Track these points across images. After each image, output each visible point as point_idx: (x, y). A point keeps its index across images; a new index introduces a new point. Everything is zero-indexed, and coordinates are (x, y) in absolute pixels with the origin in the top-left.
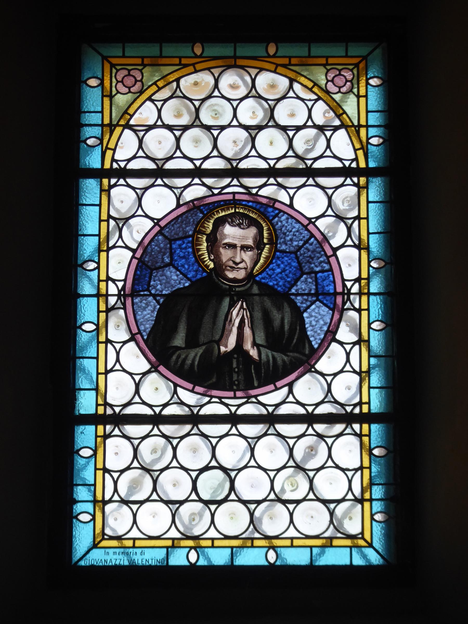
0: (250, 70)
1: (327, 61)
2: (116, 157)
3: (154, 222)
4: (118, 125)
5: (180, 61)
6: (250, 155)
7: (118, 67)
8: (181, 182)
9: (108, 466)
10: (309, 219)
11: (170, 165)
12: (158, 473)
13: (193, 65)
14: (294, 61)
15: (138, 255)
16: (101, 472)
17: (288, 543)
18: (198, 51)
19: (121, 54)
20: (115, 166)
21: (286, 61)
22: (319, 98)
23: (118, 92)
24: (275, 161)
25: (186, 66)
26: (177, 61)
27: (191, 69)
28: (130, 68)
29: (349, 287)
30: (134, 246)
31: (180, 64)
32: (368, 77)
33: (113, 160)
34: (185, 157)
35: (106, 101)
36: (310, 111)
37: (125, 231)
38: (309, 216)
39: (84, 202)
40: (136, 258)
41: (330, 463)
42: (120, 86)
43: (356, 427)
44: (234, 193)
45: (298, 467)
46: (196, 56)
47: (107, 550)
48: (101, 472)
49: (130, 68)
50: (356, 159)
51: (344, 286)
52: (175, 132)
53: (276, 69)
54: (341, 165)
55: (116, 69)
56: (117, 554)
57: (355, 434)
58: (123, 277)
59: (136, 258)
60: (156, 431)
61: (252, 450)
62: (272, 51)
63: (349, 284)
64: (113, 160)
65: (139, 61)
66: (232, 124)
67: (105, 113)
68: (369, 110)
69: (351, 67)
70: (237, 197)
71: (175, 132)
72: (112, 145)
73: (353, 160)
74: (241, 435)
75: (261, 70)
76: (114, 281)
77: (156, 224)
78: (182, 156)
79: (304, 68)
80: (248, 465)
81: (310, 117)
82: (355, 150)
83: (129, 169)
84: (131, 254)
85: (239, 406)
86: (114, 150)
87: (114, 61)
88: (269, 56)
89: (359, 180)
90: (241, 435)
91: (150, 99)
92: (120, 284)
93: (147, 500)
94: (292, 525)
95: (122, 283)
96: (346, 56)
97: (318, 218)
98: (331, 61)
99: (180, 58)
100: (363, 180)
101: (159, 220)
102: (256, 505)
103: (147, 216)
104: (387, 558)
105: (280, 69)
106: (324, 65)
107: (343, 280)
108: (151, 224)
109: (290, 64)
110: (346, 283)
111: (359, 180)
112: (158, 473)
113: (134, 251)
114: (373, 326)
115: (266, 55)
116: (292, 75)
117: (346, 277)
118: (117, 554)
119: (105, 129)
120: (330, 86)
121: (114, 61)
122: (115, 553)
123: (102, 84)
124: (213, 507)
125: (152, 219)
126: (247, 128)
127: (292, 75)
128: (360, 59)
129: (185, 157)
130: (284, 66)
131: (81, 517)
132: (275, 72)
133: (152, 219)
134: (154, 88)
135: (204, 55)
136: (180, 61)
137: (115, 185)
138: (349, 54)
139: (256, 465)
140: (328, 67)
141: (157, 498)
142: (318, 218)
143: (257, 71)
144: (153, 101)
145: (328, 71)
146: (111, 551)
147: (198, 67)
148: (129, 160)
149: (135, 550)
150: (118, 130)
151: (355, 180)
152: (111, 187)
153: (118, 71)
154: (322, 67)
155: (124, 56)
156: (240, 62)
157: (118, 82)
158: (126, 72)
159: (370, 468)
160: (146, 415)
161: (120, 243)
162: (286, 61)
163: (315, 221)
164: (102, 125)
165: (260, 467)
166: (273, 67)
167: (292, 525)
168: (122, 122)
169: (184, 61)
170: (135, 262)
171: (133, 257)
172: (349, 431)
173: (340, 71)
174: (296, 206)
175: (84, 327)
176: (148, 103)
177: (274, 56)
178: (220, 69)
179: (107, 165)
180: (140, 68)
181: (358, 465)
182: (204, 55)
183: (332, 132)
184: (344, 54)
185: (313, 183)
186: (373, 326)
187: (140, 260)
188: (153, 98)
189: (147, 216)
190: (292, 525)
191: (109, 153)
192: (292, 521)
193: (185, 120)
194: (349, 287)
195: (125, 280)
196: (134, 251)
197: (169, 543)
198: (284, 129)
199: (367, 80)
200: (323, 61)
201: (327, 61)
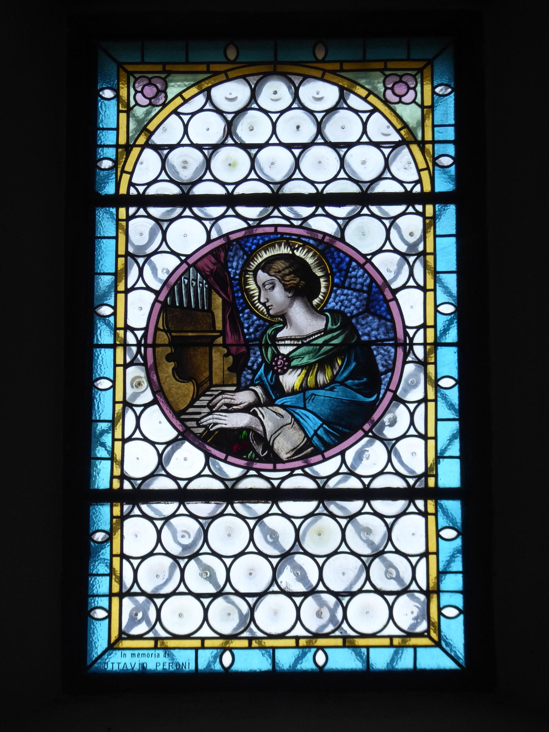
0: (293, 78)
1: (385, 65)
2: (134, 181)
3: (180, 259)
4: (135, 145)
5: (208, 68)
6: (159, 179)
7: (137, 76)
8: (215, 211)
9: (126, 552)
10: (364, 256)
11: (199, 190)
12: (363, 558)
13: (225, 72)
14: (346, 66)
15: (161, 298)
16: (119, 558)
17: (245, 643)
18: (232, 54)
19: (139, 60)
20: (133, 191)
21: (336, 66)
22: (375, 110)
23: (137, 104)
24: (324, 185)
25: (216, 73)
26: (203, 68)
27: (223, 77)
28: (400, 73)
29: (411, 336)
30: (157, 286)
31: (208, 71)
32: (435, 84)
33: (131, 184)
34: (216, 180)
35: (123, 116)
36: (365, 124)
37: (147, 270)
38: (364, 252)
39: (102, 234)
40: (159, 302)
41: (344, 548)
42: (139, 96)
43: (420, 503)
44: (276, 226)
45: (379, 554)
46: (229, 62)
47: (124, 652)
48: (119, 558)
49: (150, 76)
50: (419, 181)
51: (406, 334)
52: (383, 149)
53: (323, 75)
54: (401, 190)
55: (134, 77)
56: (136, 655)
57: (420, 513)
58: (144, 325)
59: (159, 302)
60: (182, 510)
61: (206, 532)
62: (320, 55)
63: (411, 332)
64: (131, 184)
65: (159, 68)
66: (362, 141)
67: (120, 130)
68: (435, 124)
69: (414, 73)
70: (280, 230)
71: (383, 149)
72: (129, 168)
73: (416, 182)
74: (284, 515)
75: (305, 78)
76: (133, 330)
77: (182, 262)
78: (212, 179)
79: (362, 74)
80: (339, 551)
81: (365, 132)
82: (419, 171)
83: (148, 195)
84: (152, 296)
85: (283, 479)
86: (132, 174)
87: (130, 68)
88: (318, 61)
89: (424, 209)
90: (284, 515)
91: (175, 112)
92: (140, 334)
93: (174, 593)
94: (391, 621)
95: (142, 332)
96: (409, 59)
97: (374, 254)
98: (390, 65)
99: (208, 64)
100: (429, 209)
101: (188, 256)
102: (210, 599)
103: (173, 252)
104: (93, 667)
105: (328, 76)
106: (382, 71)
107: (405, 327)
108: (177, 262)
109: (342, 70)
110: (408, 330)
111: (424, 209)
112: (363, 558)
113: (157, 293)
114: (108, 384)
115: (313, 59)
116: (345, 84)
117: (407, 324)
118: (136, 655)
119: (120, 150)
120: (389, 95)
121: (130, 68)
122: (133, 655)
123: (117, 96)
124: (158, 601)
125: (178, 255)
126: (200, 147)
127: (345, 84)
128: (425, 63)
129: (216, 180)
130: (334, 72)
131: (455, 612)
132: (322, 79)
133: (178, 255)
134: (179, 100)
135: (238, 61)
136: (208, 68)
137: (134, 216)
138: (146, 60)
139: (164, 552)
140: (387, 73)
141: (185, 590)
142: (374, 254)
143: (301, 78)
144: (178, 114)
145: (386, 77)
146: (128, 653)
147: (231, 74)
148: (149, 184)
149: (157, 652)
150: (135, 151)
151: (419, 208)
152: (129, 218)
153: (136, 80)
154: (379, 73)
155: (143, 63)
156: (280, 68)
157: (136, 92)
158: (146, 82)
159: (112, 556)
160: (398, 489)
161: (140, 284)
162: (336, 66)
163: (371, 258)
164: (117, 146)
165: (335, 553)
166: (319, 74)
167: (391, 621)
168: (142, 140)
169: (213, 68)
170: (158, 306)
171: (156, 301)
172: (412, 509)
173: (401, 77)
174: (347, 240)
175: (453, 382)
176: (174, 117)
177: (323, 61)
178: (257, 78)
179: (123, 190)
180: (163, 76)
181: (422, 549)
182: (238, 61)
183: (390, 149)
184: (184, 60)
185: (413, 211)
186: (108, 384)
187: (164, 303)
188: (180, 110)
189: (173, 252)
190: (391, 621)
191: (126, 177)
192: (391, 617)
193: (215, 138)
194: (411, 336)
195: (146, 329)
196: (157, 293)
197: (198, 643)
198: (245, 147)
199: (433, 88)
200: (381, 65)
201: (385, 65)
